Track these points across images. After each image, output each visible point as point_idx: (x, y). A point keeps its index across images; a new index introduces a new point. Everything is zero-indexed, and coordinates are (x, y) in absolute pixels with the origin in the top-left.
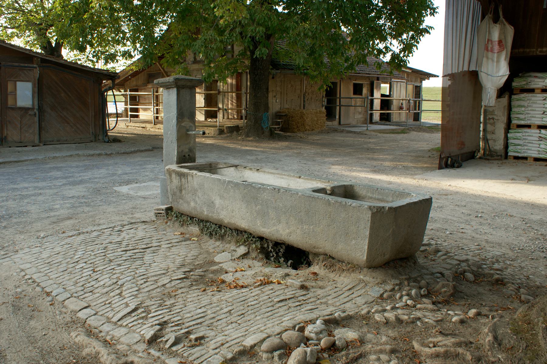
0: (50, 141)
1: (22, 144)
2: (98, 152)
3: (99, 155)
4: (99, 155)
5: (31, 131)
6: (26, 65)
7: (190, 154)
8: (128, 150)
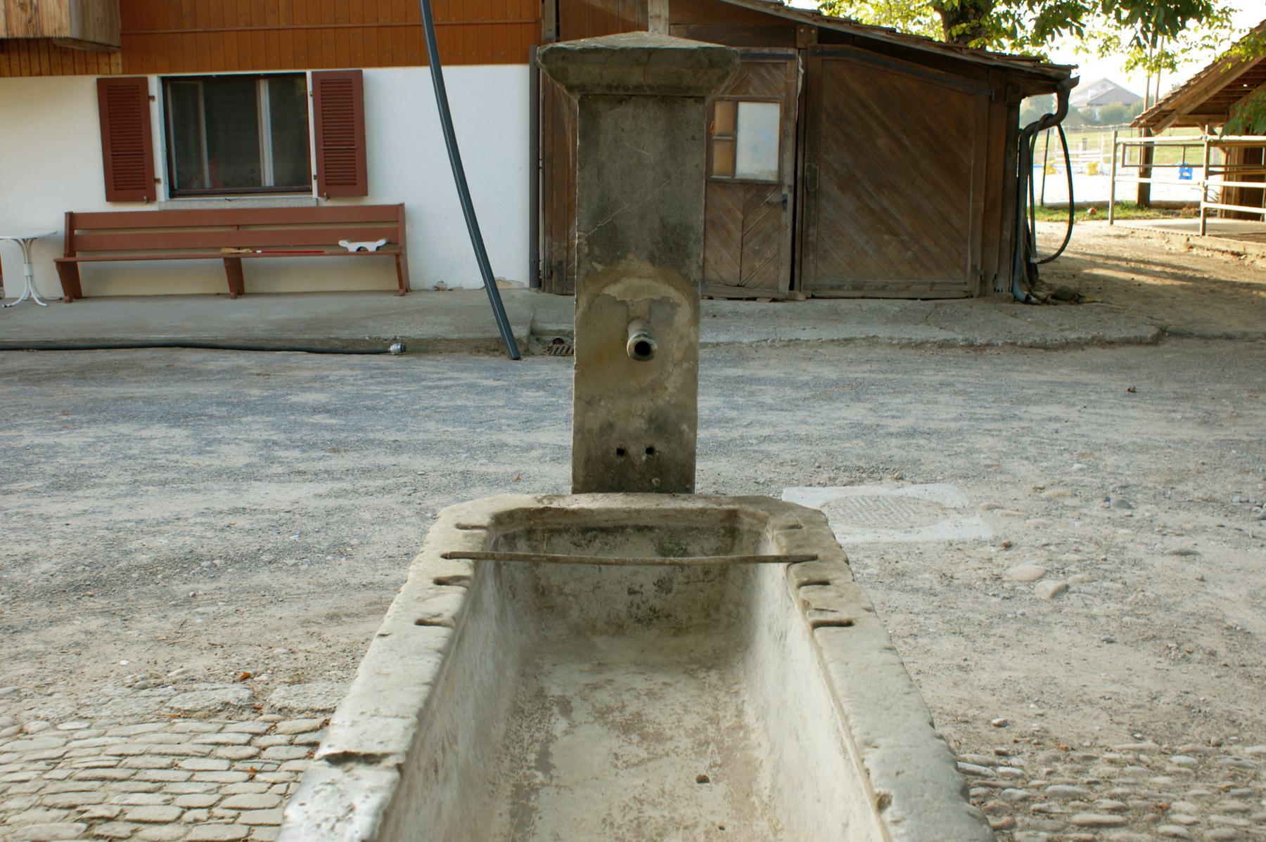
0: (832, 288)
1: (742, 292)
2: (941, 335)
3: (944, 345)
4: (944, 345)
5: (769, 255)
6: (766, 50)
7: (659, 446)
8: (1054, 336)
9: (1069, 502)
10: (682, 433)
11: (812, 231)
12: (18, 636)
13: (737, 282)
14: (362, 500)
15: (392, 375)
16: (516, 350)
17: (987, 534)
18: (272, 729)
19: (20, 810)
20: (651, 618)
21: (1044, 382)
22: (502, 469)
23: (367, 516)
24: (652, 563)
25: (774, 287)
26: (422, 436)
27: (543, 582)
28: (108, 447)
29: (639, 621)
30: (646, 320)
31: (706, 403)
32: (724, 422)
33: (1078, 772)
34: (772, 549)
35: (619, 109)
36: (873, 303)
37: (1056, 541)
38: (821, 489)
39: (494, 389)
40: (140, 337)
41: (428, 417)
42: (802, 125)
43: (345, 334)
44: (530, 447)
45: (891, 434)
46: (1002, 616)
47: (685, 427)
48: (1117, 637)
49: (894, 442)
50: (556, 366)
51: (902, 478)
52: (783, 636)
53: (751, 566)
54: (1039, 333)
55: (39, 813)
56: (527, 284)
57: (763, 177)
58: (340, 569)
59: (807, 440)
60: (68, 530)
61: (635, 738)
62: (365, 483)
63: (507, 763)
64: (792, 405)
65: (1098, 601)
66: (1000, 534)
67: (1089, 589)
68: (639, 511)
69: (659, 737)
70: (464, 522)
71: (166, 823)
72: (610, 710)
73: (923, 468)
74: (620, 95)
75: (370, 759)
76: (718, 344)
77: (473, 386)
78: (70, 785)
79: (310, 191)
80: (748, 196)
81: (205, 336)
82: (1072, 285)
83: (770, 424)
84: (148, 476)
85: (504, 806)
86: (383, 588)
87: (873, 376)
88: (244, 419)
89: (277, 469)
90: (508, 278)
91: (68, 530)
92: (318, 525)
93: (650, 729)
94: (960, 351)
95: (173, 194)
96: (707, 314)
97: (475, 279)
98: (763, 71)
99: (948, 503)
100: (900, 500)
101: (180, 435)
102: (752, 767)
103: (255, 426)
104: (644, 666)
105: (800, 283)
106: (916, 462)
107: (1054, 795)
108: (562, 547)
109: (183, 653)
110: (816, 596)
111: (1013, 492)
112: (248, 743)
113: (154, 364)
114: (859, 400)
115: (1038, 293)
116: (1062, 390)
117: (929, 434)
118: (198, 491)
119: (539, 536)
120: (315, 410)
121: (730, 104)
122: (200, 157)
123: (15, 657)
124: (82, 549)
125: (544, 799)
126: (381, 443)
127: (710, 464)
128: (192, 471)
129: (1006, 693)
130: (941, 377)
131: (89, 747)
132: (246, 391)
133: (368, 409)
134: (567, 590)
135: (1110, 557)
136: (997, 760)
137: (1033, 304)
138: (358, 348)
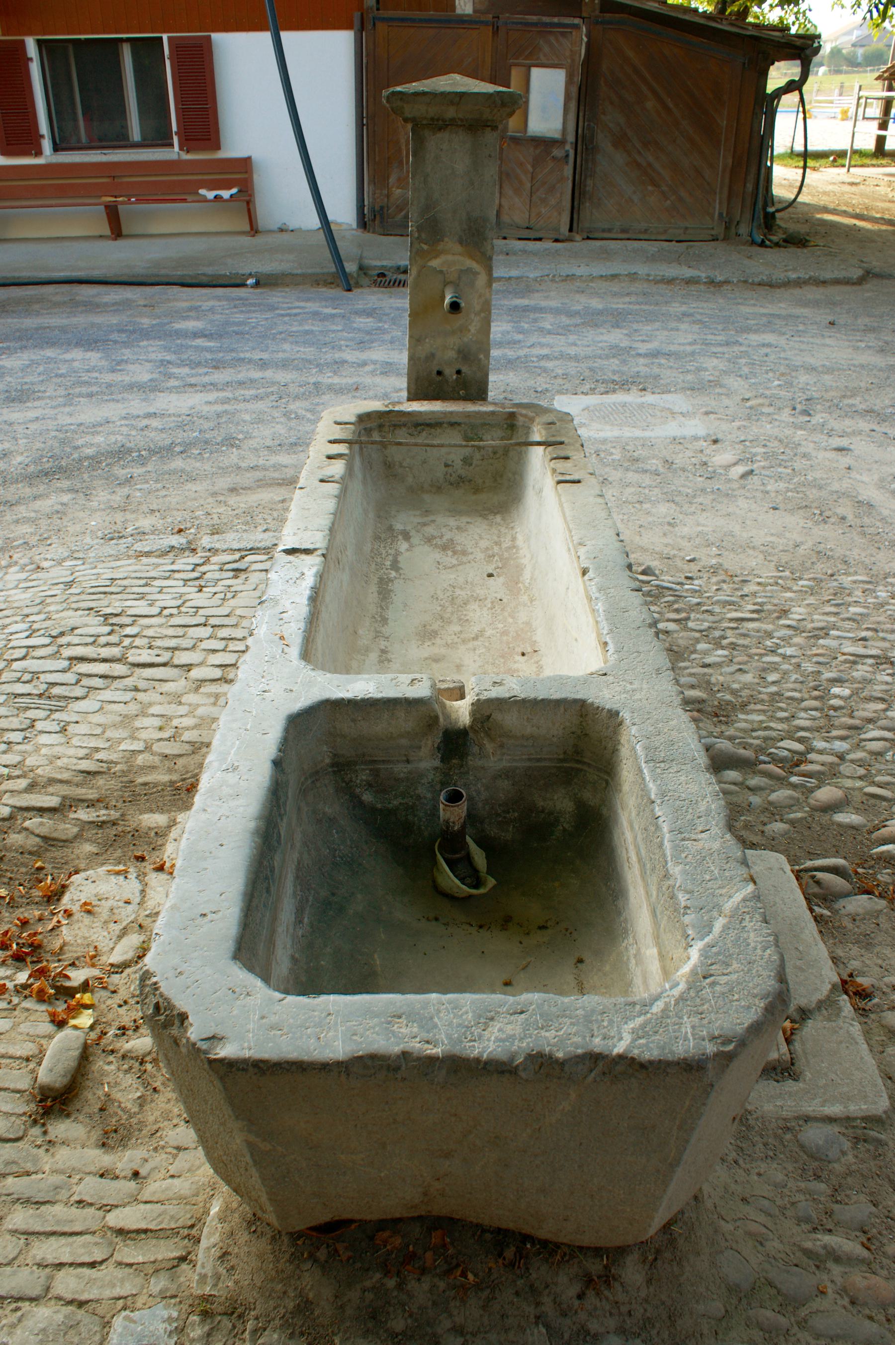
0: (604, 231)
2: (688, 273)
4: (690, 282)
6: (556, 20)
7: (464, 369)
8: (779, 275)
9: (766, 410)
10: (480, 360)
11: (589, 182)
12: (14, 508)
13: (526, 225)
14: (242, 406)
15: (251, 305)
16: (347, 282)
17: (701, 432)
18: (207, 561)
19: (58, 612)
20: (460, 482)
21: (765, 315)
22: (344, 381)
23: (247, 417)
24: (461, 446)
25: (557, 229)
26: (281, 355)
27: (389, 459)
28: (41, 369)
29: (451, 484)
30: (456, 285)
31: (499, 328)
32: (513, 343)
33: (736, 589)
34: (537, 438)
35: (439, 135)
36: (636, 244)
37: (751, 438)
38: (583, 397)
39: (333, 316)
40: (44, 275)
41: (284, 339)
42: (583, 88)
43: (209, 270)
44: (364, 364)
45: (640, 355)
46: (703, 490)
47: (482, 356)
48: (781, 506)
49: (642, 361)
50: (380, 296)
51: (644, 390)
52: (541, 491)
53: (524, 448)
54: (767, 273)
55: (71, 613)
56: (355, 226)
57: (550, 135)
58: (233, 457)
59: (576, 358)
60: (29, 432)
61: (450, 553)
62: (242, 392)
63: (373, 566)
64: (565, 330)
65: (772, 481)
66: (711, 432)
67: (767, 473)
68: (451, 413)
69: (464, 553)
70: (339, 420)
71: (153, 616)
72: (434, 537)
73: (662, 382)
74: (440, 125)
75: (307, 552)
76: (510, 278)
77: (316, 314)
78: (83, 597)
79: (171, 145)
80: (537, 152)
81: (96, 274)
82: (803, 229)
83: (548, 345)
84: (77, 390)
85: (373, 588)
86: (266, 470)
87: (631, 307)
88: (141, 344)
89: (173, 383)
90: (339, 220)
91: (29, 432)
92: (211, 424)
93: (459, 548)
94: (702, 287)
95: (56, 148)
96: (501, 252)
97: (314, 222)
98: (552, 39)
99: (676, 409)
100: (641, 406)
101: (94, 357)
102: (520, 569)
103: (151, 349)
104: (455, 512)
105: (578, 227)
106: (657, 377)
107: (718, 602)
108: (402, 436)
109: (134, 516)
110: (560, 465)
111: (726, 401)
112: (193, 570)
113: (58, 298)
114: (618, 327)
115: (772, 238)
116: (777, 321)
117: (669, 355)
118: (118, 401)
119: (386, 429)
120: (196, 335)
121: (523, 69)
122: (75, 113)
123: (17, 522)
124: (43, 445)
125: (397, 586)
126: (250, 361)
127: (501, 377)
128: (109, 386)
129: (698, 541)
130: (684, 308)
131: (87, 576)
132: (138, 320)
133: (237, 333)
134: (405, 464)
135: (788, 451)
136: (685, 581)
137: (766, 247)
138: (221, 282)
